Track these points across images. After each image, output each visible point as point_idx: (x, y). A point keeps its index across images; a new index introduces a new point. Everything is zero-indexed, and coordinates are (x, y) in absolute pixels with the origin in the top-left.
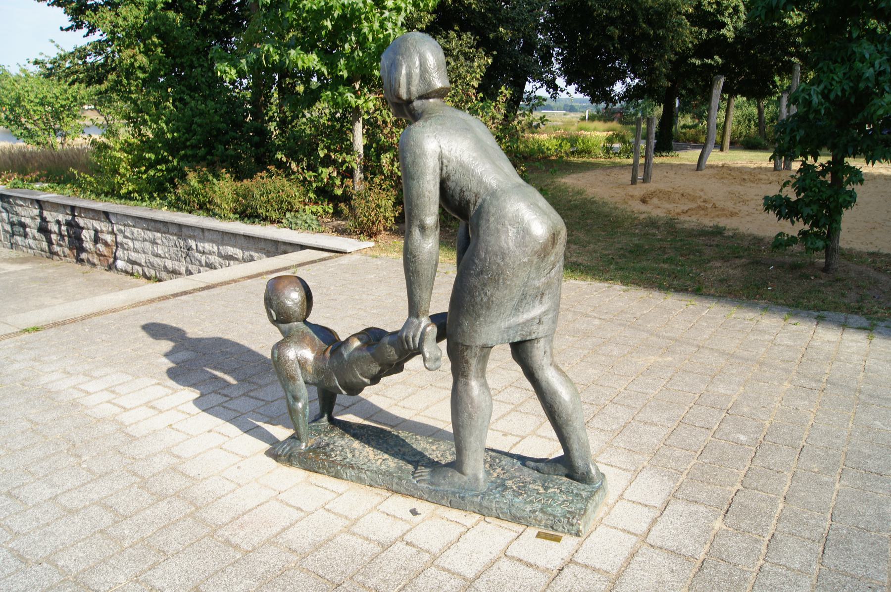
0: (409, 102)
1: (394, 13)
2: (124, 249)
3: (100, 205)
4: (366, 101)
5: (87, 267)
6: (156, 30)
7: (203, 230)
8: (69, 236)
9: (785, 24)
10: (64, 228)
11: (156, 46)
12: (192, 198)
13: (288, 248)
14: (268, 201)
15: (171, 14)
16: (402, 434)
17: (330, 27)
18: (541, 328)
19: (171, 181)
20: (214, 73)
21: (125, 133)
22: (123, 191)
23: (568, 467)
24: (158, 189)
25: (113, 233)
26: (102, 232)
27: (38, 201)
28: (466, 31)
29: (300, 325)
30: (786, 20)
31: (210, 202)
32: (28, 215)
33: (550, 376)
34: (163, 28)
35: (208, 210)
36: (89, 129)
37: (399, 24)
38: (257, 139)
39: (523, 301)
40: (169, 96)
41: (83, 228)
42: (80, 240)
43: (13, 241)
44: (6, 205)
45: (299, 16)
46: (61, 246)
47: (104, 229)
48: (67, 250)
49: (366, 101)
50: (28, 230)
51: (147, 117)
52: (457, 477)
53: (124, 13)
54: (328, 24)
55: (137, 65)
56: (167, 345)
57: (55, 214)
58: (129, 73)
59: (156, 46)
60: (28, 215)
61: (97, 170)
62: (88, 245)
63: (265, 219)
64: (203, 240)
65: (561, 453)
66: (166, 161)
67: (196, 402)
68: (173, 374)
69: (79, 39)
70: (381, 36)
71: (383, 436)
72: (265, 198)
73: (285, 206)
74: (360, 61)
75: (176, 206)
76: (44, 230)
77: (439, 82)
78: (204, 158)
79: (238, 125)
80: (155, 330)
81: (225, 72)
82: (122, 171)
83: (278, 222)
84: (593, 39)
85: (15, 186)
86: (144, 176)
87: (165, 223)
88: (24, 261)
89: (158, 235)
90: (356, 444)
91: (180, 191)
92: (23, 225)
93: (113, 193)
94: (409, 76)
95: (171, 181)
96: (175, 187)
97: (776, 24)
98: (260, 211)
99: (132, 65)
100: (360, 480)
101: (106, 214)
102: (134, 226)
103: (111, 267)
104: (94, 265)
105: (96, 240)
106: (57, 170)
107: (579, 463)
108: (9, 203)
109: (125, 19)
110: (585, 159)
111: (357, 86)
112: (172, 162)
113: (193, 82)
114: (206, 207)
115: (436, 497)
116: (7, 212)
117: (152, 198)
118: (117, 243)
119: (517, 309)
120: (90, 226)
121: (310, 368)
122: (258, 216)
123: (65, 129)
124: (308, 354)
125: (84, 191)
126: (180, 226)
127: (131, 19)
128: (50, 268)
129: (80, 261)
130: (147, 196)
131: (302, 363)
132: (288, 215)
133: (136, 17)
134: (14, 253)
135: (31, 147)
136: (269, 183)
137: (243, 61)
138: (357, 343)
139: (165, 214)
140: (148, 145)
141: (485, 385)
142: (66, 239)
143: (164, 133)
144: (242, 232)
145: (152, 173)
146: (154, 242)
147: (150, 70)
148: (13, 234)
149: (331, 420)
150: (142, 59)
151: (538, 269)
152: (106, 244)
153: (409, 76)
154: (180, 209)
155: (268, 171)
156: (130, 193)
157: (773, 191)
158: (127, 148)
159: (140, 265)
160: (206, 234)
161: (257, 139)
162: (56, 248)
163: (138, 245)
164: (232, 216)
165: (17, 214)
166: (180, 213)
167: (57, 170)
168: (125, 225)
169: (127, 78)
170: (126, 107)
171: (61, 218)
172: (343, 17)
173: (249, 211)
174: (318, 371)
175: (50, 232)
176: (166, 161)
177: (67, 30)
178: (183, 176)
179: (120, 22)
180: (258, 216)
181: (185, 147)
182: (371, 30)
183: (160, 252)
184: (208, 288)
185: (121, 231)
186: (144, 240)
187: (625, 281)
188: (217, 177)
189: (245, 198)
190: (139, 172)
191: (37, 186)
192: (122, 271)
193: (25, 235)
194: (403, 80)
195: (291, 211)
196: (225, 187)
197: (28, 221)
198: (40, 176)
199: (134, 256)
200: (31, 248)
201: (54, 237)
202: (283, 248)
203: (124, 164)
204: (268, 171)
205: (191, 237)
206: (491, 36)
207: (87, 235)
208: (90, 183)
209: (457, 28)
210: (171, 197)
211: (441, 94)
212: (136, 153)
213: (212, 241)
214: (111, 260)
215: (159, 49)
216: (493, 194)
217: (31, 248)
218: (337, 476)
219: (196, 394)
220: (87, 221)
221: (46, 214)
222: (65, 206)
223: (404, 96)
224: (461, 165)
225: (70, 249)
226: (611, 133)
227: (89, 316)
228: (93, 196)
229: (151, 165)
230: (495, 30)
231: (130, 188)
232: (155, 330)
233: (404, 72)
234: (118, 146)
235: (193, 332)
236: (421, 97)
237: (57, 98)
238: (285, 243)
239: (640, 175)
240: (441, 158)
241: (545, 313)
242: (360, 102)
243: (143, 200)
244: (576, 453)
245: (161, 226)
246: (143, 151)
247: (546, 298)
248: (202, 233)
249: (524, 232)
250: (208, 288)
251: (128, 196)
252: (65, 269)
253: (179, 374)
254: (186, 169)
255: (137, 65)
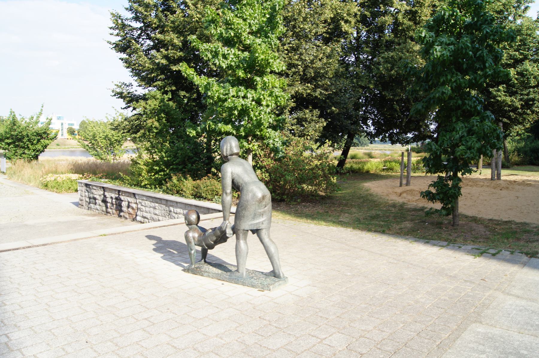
0: (227, 157)
1: (266, 108)
2: (141, 211)
3: (132, 190)
4: (253, 146)
5: (123, 219)
6: (163, 111)
7: (177, 202)
8: (116, 205)
9: (498, 100)
10: (114, 200)
11: (163, 118)
12: (174, 188)
13: (214, 211)
14: (207, 191)
15: (171, 103)
16: (227, 266)
17: (237, 114)
18: (263, 226)
19: (165, 180)
20: (186, 133)
21: (146, 156)
22: (143, 184)
23: (274, 274)
24: (159, 183)
25: (136, 203)
26: (131, 203)
27: (103, 188)
28: (315, 109)
29: (195, 226)
30: (498, 98)
31: (182, 190)
32: (98, 194)
33: (266, 240)
34: (166, 110)
35: (180, 194)
36: (128, 153)
37: (267, 112)
38: (207, 161)
39: (255, 217)
40: (167, 140)
41: (122, 201)
42: (121, 206)
43: (89, 206)
44: (88, 189)
45: (223, 109)
46: (112, 209)
47: (133, 201)
48: (114, 211)
49: (253, 146)
50: (97, 201)
51: (156, 150)
52: (237, 274)
53: (150, 103)
54: (236, 112)
55: (153, 126)
56: (154, 242)
57: (110, 194)
58: (150, 130)
59: (163, 118)
60: (98, 194)
61: (132, 174)
62: (124, 209)
63: (205, 199)
64: (177, 207)
65: (272, 269)
66: (164, 171)
67: (162, 257)
68: (155, 250)
69: (129, 113)
70: (258, 118)
71: (220, 265)
72: (205, 189)
73: (215, 193)
74: (250, 128)
75: (166, 192)
76: (104, 201)
77: (235, 151)
78: (181, 170)
79: (197, 154)
80: (150, 237)
81: (191, 132)
82: (143, 174)
83: (212, 200)
84: (386, 111)
85: (93, 181)
86: (153, 177)
87: (160, 199)
88: (94, 215)
89: (157, 205)
90: (211, 267)
91: (168, 185)
92: (95, 199)
93: (138, 185)
94: (227, 149)
95: (165, 180)
96: (167, 183)
97: (492, 100)
98: (203, 195)
99: (151, 126)
100: (209, 276)
101: (134, 194)
102: (145, 201)
103: (134, 220)
104: (126, 218)
105: (128, 207)
106: (113, 173)
107: (277, 271)
108: (89, 188)
109: (150, 106)
110: (390, 173)
111: (250, 139)
112: (166, 171)
113: (179, 134)
114: (179, 192)
115: (230, 280)
116: (88, 192)
117: (156, 188)
118: (138, 208)
119: (254, 218)
120: (126, 200)
121: (196, 240)
122: (202, 197)
123: (115, 152)
124: (196, 235)
125: (125, 183)
126: (167, 201)
127: (153, 106)
128: (106, 219)
129: (120, 216)
130: (153, 187)
131: (194, 238)
132: (216, 197)
133: (155, 105)
134: (89, 212)
135: (99, 161)
136: (208, 183)
137: (199, 128)
138: (211, 231)
139: (161, 195)
140: (156, 163)
141: (246, 243)
142: (115, 206)
143: (164, 158)
144: (194, 204)
145: (157, 176)
146: (155, 208)
147: (160, 128)
148: (90, 203)
149: (205, 261)
150: (156, 124)
151: (259, 206)
152: (133, 209)
153: (227, 149)
154: (168, 193)
155: (208, 176)
156: (146, 185)
157: (425, 188)
158: (146, 164)
159: (147, 219)
160: (178, 204)
161: (207, 161)
162: (109, 210)
163: (147, 209)
164: (191, 197)
165: (93, 193)
166: (167, 195)
167: (113, 173)
168: (142, 200)
169: (149, 132)
170: (148, 144)
171: (114, 196)
172: (242, 110)
173: (198, 194)
174: (199, 241)
175: (107, 202)
176: (164, 171)
177: (124, 109)
178: (170, 178)
179: (148, 107)
180: (202, 197)
181: (173, 164)
182: (255, 115)
183: (157, 213)
184: (174, 225)
185: (140, 203)
186: (151, 207)
187: (354, 228)
188: (186, 178)
189: (197, 188)
190: (151, 176)
191: (103, 180)
192: (139, 221)
193: (95, 204)
194: (225, 150)
195: (217, 195)
196: (189, 183)
197: (97, 197)
198: (103, 176)
199: (145, 214)
200: (97, 210)
201: (109, 205)
202: (211, 211)
203: (144, 172)
204: (208, 176)
205: (171, 206)
206: (328, 111)
207: (124, 204)
208: (128, 180)
209: (311, 107)
210: (164, 188)
211: (237, 154)
212: (151, 166)
213: (181, 208)
214: (134, 216)
215: (164, 119)
216: (246, 183)
217: (97, 210)
218: (202, 275)
219: (162, 255)
220: (125, 197)
221: (106, 193)
222: (115, 190)
223: (225, 155)
224: (238, 175)
225: (116, 210)
226: (419, 158)
227: (125, 232)
228: (129, 186)
229: (157, 172)
230: (330, 108)
231: (146, 183)
232: (150, 237)
233: (225, 148)
234: (142, 163)
235: (164, 238)
236: (230, 155)
237: (113, 136)
238: (212, 209)
239: (404, 182)
240: (232, 173)
241: (264, 221)
242: (251, 146)
243: (151, 188)
244: (276, 268)
245: (158, 201)
246: (154, 165)
247: (264, 216)
248: (177, 204)
249: (254, 195)
250: (174, 225)
251: (145, 187)
252: (113, 219)
253: (157, 250)
254: (172, 174)
255: (153, 126)
